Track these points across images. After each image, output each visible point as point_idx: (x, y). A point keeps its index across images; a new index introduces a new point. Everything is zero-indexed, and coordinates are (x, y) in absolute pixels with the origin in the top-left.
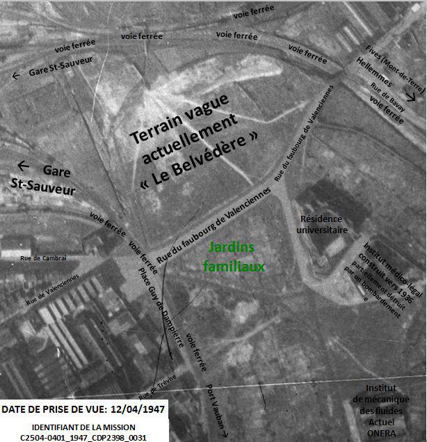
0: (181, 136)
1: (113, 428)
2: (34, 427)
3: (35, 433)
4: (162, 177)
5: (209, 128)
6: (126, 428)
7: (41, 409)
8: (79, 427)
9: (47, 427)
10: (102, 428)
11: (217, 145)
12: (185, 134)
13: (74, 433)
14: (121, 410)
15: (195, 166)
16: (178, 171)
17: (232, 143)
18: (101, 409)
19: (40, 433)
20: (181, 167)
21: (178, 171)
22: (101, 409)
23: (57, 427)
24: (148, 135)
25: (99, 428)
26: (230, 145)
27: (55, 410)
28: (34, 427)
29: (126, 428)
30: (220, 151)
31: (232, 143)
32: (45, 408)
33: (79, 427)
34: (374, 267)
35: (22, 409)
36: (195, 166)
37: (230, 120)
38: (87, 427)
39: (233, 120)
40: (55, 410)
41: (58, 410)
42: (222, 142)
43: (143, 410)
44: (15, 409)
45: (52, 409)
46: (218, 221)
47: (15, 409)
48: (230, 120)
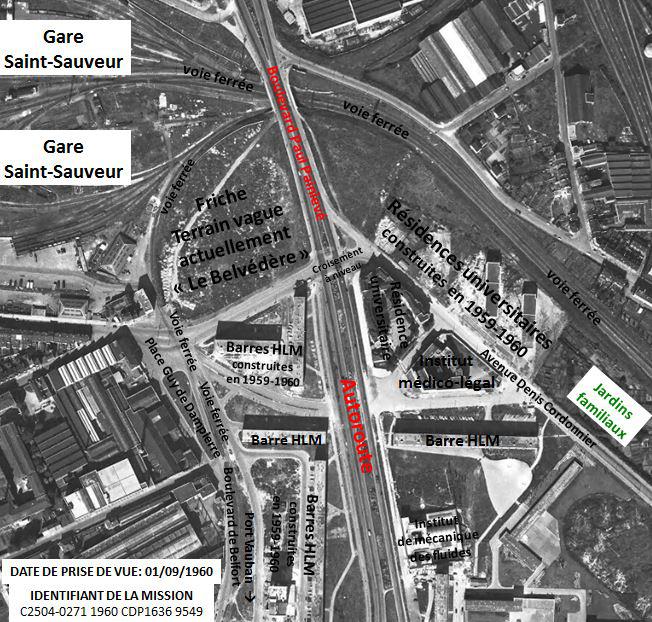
0: (226, 242)
1: (158, 596)
2: (34, 595)
3: (35, 603)
4: (199, 283)
5: (258, 238)
6: (180, 596)
7: (59, 571)
8: (104, 595)
9: (55, 596)
10: (140, 595)
11: (264, 258)
12: (231, 241)
13: (97, 603)
14: (159, 573)
15: (236, 277)
16: (217, 279)
17: (281, 258)
18: (132, 572)
19: (42, 603)
20: (221, 275)
21: (217, 279)
22: (133, 572)
23: (71, 595)
24: (246, 246)
25: (134, 595)
26: (273, 237)
27: (76, 572)
28: (34, 595)
29: (180, 596)
30: (266, 265)
31: (281, 258)
32: (179, 611)
33: (104, 595)
34: (260, 366)
35: (35, 571)
36: (236, 277)
37: (283, 233)
38: (117, 595)
39: (286, 234)
40: (76, 572)
41: (158, 596)
42: (271, 255)
43: (186, 572)
44: (27, 570)
45: (71, 571)
46: (616, 401)
47: (27, 570)
48: (283, 233)
